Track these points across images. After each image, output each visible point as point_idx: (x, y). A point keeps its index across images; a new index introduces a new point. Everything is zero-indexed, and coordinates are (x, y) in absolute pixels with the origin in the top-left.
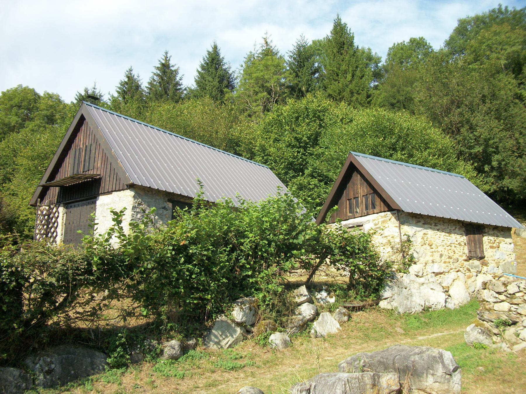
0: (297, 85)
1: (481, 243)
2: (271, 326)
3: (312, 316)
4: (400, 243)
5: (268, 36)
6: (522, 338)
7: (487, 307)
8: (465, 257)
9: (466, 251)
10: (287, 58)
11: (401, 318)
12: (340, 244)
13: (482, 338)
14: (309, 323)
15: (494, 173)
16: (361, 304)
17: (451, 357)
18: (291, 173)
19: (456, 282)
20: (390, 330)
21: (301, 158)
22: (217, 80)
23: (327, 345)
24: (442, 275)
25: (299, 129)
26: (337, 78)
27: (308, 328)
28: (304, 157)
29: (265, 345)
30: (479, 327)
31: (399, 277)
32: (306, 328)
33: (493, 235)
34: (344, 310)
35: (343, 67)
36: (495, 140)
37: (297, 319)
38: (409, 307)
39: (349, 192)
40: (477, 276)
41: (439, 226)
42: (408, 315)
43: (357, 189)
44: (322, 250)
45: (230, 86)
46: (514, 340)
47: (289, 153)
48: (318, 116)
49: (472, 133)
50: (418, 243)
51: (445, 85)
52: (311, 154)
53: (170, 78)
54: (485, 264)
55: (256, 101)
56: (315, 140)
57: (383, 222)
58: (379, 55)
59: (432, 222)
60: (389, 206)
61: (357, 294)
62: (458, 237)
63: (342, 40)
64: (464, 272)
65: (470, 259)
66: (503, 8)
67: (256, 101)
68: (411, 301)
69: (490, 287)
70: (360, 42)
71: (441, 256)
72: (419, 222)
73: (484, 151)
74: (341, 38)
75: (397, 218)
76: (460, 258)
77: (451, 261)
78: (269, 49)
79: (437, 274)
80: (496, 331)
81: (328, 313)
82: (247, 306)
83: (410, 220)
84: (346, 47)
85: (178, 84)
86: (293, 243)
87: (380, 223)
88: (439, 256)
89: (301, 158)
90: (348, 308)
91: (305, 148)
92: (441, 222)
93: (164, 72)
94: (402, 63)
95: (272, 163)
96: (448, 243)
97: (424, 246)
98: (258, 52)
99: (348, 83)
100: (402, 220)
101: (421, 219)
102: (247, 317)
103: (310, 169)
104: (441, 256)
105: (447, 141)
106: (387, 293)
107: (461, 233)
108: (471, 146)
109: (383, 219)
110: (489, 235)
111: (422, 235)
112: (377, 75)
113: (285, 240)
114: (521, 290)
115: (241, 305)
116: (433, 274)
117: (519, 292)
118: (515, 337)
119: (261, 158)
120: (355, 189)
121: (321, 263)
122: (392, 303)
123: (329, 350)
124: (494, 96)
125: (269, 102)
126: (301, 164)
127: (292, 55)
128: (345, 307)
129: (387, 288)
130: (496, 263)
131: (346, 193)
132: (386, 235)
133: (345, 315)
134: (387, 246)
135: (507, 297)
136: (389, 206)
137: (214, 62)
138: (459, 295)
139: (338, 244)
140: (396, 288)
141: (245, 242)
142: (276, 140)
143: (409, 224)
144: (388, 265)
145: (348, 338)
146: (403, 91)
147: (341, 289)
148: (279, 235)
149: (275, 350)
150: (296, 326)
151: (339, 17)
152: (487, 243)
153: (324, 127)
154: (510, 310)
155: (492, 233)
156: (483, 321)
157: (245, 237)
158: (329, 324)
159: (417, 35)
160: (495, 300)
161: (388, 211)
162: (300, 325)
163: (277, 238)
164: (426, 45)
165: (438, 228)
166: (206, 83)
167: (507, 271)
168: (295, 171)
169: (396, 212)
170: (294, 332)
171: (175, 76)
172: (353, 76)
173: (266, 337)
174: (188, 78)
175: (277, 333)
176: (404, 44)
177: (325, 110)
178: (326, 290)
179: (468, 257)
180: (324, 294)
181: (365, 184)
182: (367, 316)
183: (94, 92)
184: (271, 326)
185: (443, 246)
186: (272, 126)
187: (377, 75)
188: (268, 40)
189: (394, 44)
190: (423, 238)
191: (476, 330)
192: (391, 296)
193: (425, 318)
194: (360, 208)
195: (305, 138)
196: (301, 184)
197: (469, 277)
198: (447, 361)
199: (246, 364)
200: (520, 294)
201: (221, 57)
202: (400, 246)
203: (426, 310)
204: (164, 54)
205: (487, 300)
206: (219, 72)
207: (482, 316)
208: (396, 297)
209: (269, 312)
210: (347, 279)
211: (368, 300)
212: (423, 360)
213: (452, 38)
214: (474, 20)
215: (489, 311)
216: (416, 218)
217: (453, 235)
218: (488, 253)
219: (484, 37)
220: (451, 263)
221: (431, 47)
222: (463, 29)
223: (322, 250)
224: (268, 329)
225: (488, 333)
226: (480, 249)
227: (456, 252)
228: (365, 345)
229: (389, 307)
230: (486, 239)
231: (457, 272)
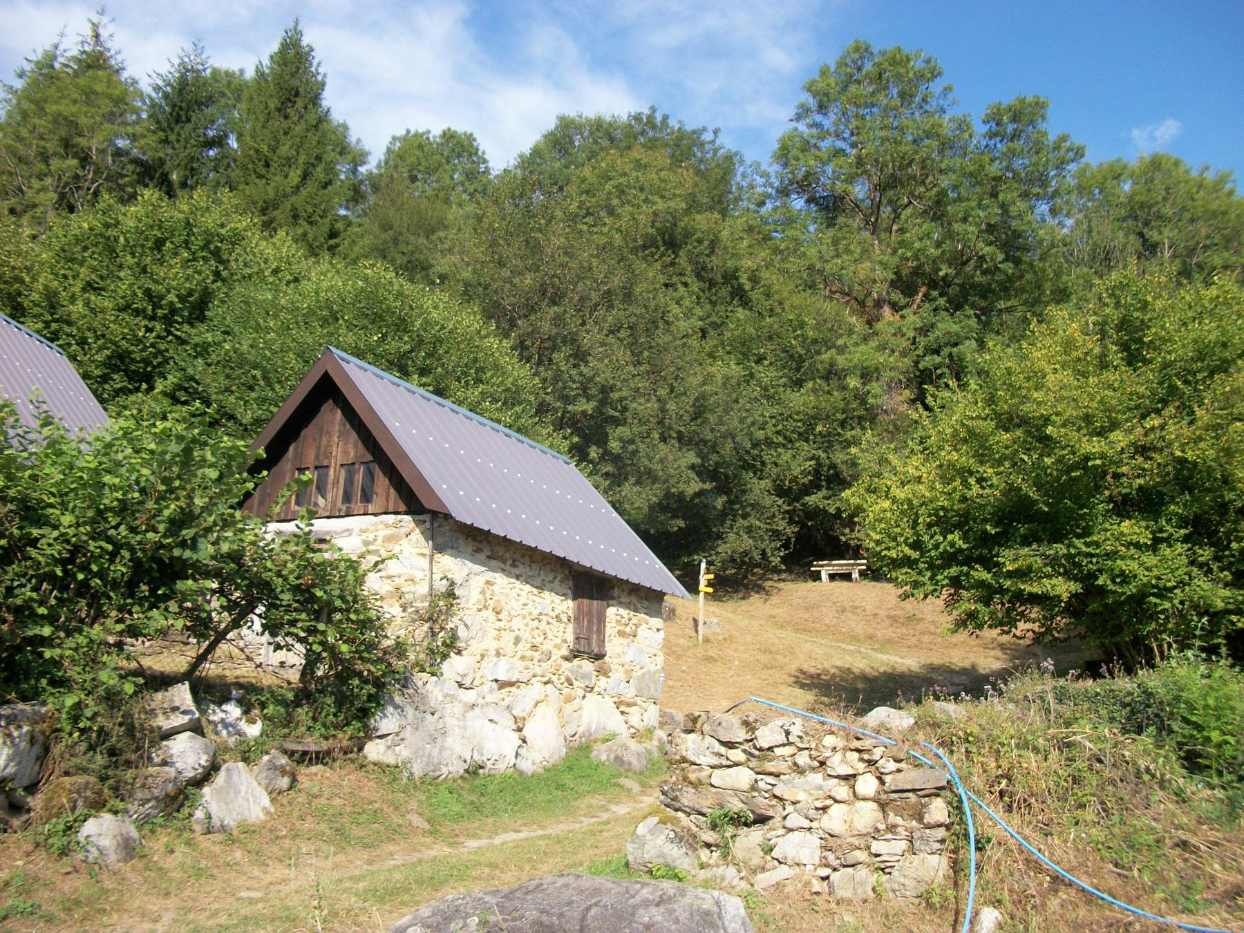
1: (601, 620)
2: (89, 793)
3: (200, 770)
4: (429, 598)
6: (780, 857)
7: (693, 777)
8: (565, 651)
9: (570, 637)
11: (415, 787)
12: (297, 578)
13: (677, 855)
14: (191, 790)
15: (609, 468)
16: (325, 745)
17: (742, 912)
18: (118, 381)
19: (541, 707)
20: (397, 820)
21: (153, 345)
23: (238, 854)
24: (513, 689)
26: (264, 171)
27: (187, 803)
29: (64, 852)
30: (669, 825)
31: (420, 684)
32: (182, 805)
33: (627, 606)
34: (284, 760)
35: (285, 150)
36: (624, 393)
37: (159, 778)
38: (436, 761)
39: (306, 448)
40: (584, 697)
41: (521, 567)
42: (431, 781)
43: (329, 445)
44: (251, 588)
46: (756, 861)
48: (215, 250)
49: (575, 366)
50: (471, 602)
51: (535, 248)
52: (183, 342)
54: (603, 672)
55: (41, 177)
56: (198, 309)
57: (388, 539)
58: (367, 145)
59: (507, 555)
60: (412, 500)
61: (314, 719)
62: (557, 599)
63: (294, 82)
64: (560, 686)
65: (575, 657)
66: (659, 117)
67: (41, 177)
68: (443, 748)
69: (706, 728)
70: (338, 103)
71: (517, 640)
72: (479, 550)
73: (599, 410)
74: (292, 83)
75: (429, 533)
76: (555, 651)
77: (537, 655)
78: (101, 53)
79: (503, 685)
80: (709, 836)
81: (241, 764)
82: (25, 729)
83: (461, 542)
84: (300, 103)
86: (179, 558)
87: (379, 541)
88: (512, 640)
89: (153, 345)
90: (291, 754)
91: (168, 321)
92: (527, 560)
94: (413, 179)
95: (69, 345)
96: (536, 612)
97: (484, 613)
98: (68, 54)
99: (289, 190)
100: (440, 540)
101: (485, 543)
102: (19, 763)
103: (172, 379)
104: (517, 640)
105: (520, 373)
106: (387, 722)
107: (565, 591)
108: (568, 397)
109: (388, 532)
110: (620, 604)
111: (482, 585)
112: (356, 195)
113: (162, 546)
114: (791, 739)
115: (8, 724)
116: (495, 685)
117: (784, 745)
118: (762, 854)
119: (40, 325)
120: (324, 443)
121: (235, 624)
122: (397, 748)
123: (246, 869)
124: (628, 296)
125: (78, 188)
126: (147, 362)
127: (161, 83)
128: (285, 752)
129: (390, 709)
130: (626, 672)
131: (296, 450)
132: (390, 572)
133: (284, 772)
134: (391, 601)
135: (751, 755)
136: (412, 500)
138: (546, 744)
139: (291, 578)
140: (410, 711)
141: (43, 536)
143: (457, 552)
144: (400, 649)
145: (293, 838)
146: (408, 244)
147: (283, 702)
148: (147, 531)
149: (95, 869)
150: (156, 798)
151: (299, 28)
152: (613, 624)
153: (224, 280)
154: (754, 788)
155: (627, 600)
156: (676, 810)
158: (241, 796)
159: (460, 128)
160: (715, 761)
161: (406, 513)
162: (167, 795)
163: (139, 538)
164: (476, 154)
165: (517, 571)
167: (646, 693)
168: (132, 376)
169: (426, 517)
170: (148, 815)
172: (305, 177)
173: (70, 828)
175: (107, 817)
176: (428, 138)
177: (236, 239)
178: (240, 702)
179: (572, 651)
180: (233, 711)
181: (354, 435)
182: (336, 778)
184: (89, 793)
185: (524, 617)
186: (85, 249)
187: (356, 195)
188: (102, 31)
189: (408, 131)
190: (483, 592)
191: (662, 832)
192: (397, 730)
193: (471, 791)
194: (329, 496)
195: (172, 297)
197: (569, 699)
198: (733, 925)
199: (12, 907)
200: (788, 751)
202: (427, 604)
203: (473, 771)
205: (692, 758)
207: (675, 799)
208: (407, 733)
209: (85, 753)
210: (294, 676)
211: (340, 735)
212: (677, 921)
213: (536, 152)
214: (591, 126)
215: (695, 787)
216: (474, 539)
217: (546, 594)
218: (614, 646)
219: (613, 166)
220: (535, 661)
221: (485, 161)
222: (562, 139)
223: (251, 588)
224: (80, 803)
225: (689, 840)
226: (598, 636)
227: (550, 635)
228: (341, 858)
229: (391, 760)
230: (614, 614)
231: (546, 683)
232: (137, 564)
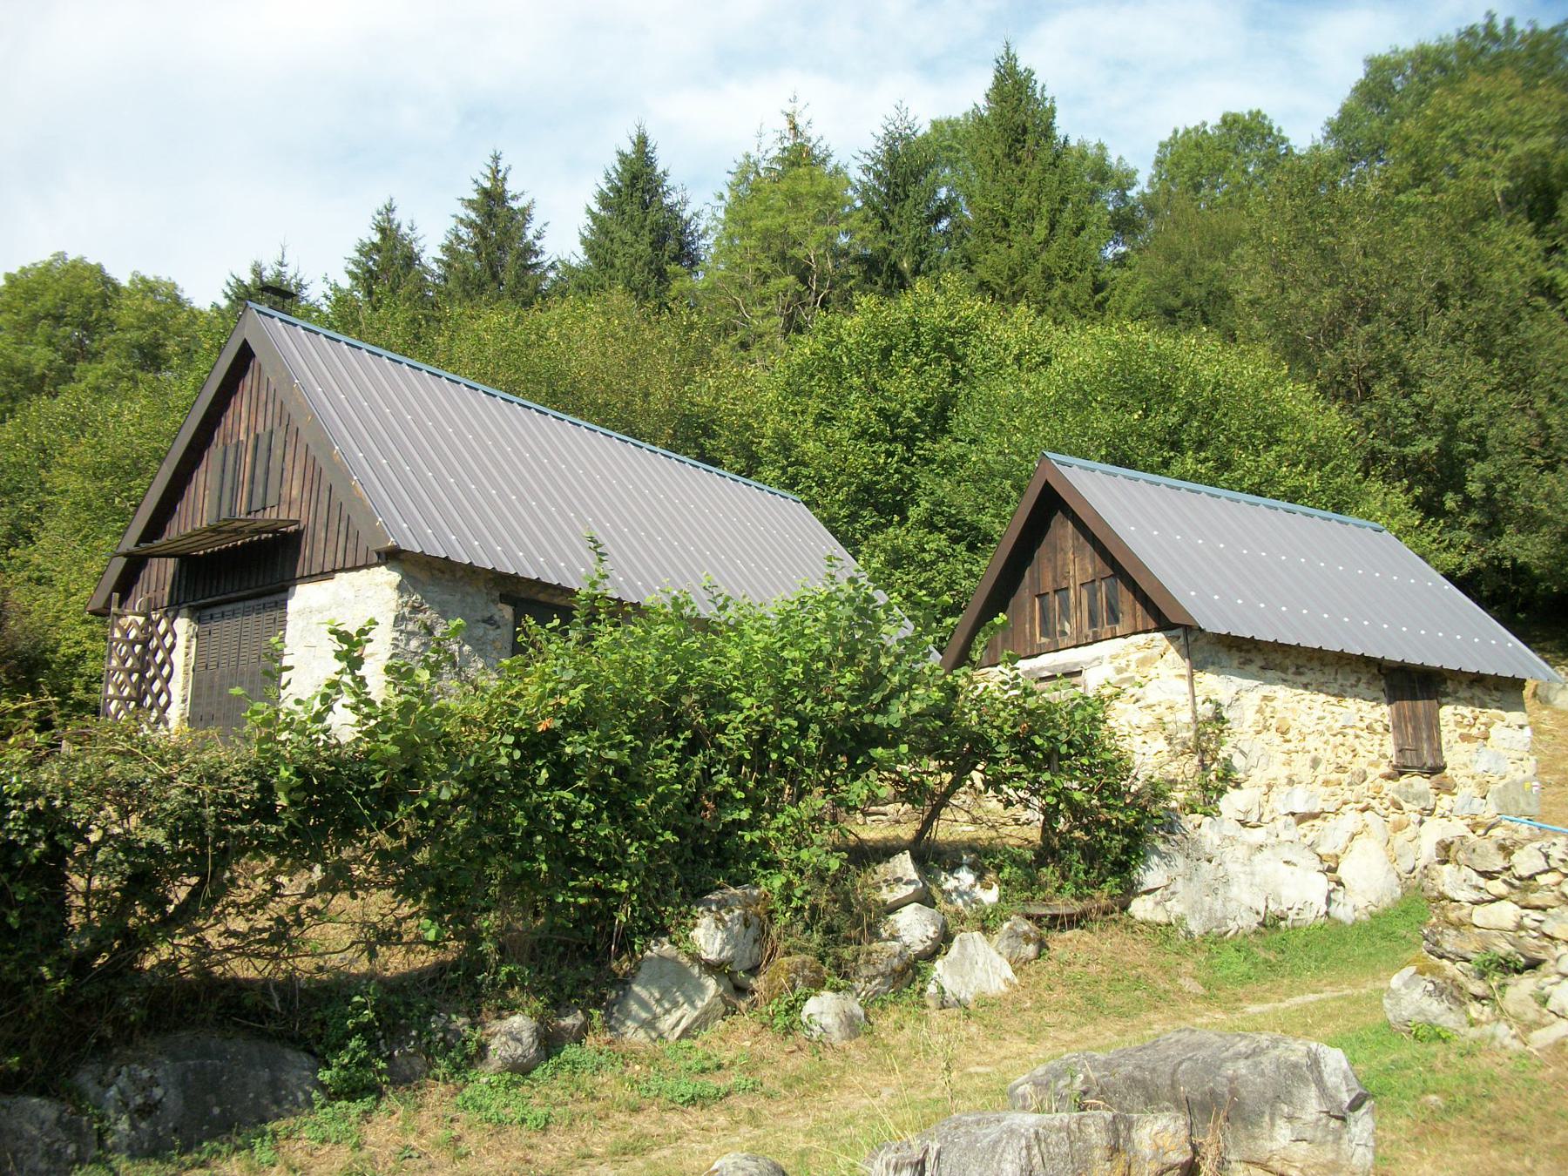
0: (887, 253)
1: (1434, 725)
2: (807, 972)
3: (929, 943)
4: (1193, 727)
5: (799, 106)
6: (1556, 1009)
7: (1452, 916)
8: (1385, 769)
9: (1390, 749)
10: (855, 174)
11: (1195, 949)
12: (1013, 727)
13: (1436, 1008)
14: (921, 964)
15: (1474, 517)
16: (1077, 907)
17: (1345, 1065)
18: (868, 517)
19: (1358, 841)
20: (1163, 985)
21: (897, 471)
22: (647, 240)
23: (974, 1029)
24: (1317, 822)
25: (890, 386)
26: (1004, 233)
27: (919, 978)
28: (907, 470)
29: (789, 1030)
30: (1428, 976)
31: (1189, 827)
32: (913, 980)
33: (1469, 702)
34: (1026, 926)
35: (1024, 201)
36: (1477, 419)
37: (885, 952)
38: (1219, 915)
39: (1041, 573)
40: (1421, 822)
41: (1309, 673)
42: (1215, 940)
43: (1065, 565)
44: (959, 746)
45: (687, 256)
46: (1531, 1015)
47: (861, 458)
48: (947, 346)
49: (1406, 396)
50: (1246, 725)
51: (1327, 255)
52: (928, 461)
53: (506, 232)
54: (1446, 788)
55: (763, 301)
56: (938, 417)
57: (1143, 662)
58: (1131, 163)
59: (1288, 662)
60: (1160, 615)
61: (1064, 877)
62: (1366, 706)
63: (1018, 119)
64: (1384, 812)
65: (1402, 774)
66: (1500, 24)
67: (763, 301)
68: (1226, 900)
69: (1461, 856)
70: (1073, 126)
71: (1315, 763)
72: (1250, 661)
73: (1444, 451)
74: (1017, 115)
75: (1184, 650)
76: (1370, 770)
77: (1345, 778)
78: (802, 145)
79: (1302, 818)
80: (1477, 987)
81: (977, 934)
82: (737, 912)
83: (1223, 656)
84: (1030, 140)
85: (530, 250)
86: (872, 724)
87: (1133, 666)
88: (1309, 763)
89: (897, 471)
90: (1037, 920)
91: (909, 442)
92: (1316, 664)
93: (490, 216)
94: (1197, 187)
95: (810, 488)
96: (1337, 726)
97: (1265, 735)
98: (769, 156)
99: (1037, 248)
100: (1198, 657)
101: (1254, 652)
102: (735, 946)
103: (924, 504)
104: (1315, 763)
105: (1332, 421)
106: (1152, 875)
107: (1375, 695)
108: (1403, 436)
109: (1141, 655)
110: (1458, 700)
111: (1257, 701)
112: (1124, 224)
113: (850, 715)
114: (1553, 864)
115: (719, 909)
116: (1291, 819)
117: (1546, 872)
118: (1536, 1006)
119: (778, 472)
120: (1059, 563)
121: (956, 784)
122: (1168, 904)
123: (979, 1044)
124: (1472, 287)
125: (803, 305)
126: (896, 490)
127: (870, 163)
128: (1029, 917)
129: (1155, 859)
130: (1480, 785)
131: (1032, 577)
132: (1150, 702)
133: (1028, 940)
134: (1154, 734)
135: (1511, 885)
136: (1160, 615)
137: (637, 184)
138: (1370, 881)
139: (1006, 728)
140: (1180, 860)
141: (730, 721)
142: (823, 419)
143: (1220, 669)
144: (1157, 792)
145: (1038, 1010)
146: (1203, 271)
147: (1016, 861)
148: (833, 701)
149: (820, 1045)
150: (883, 974)
151: (1012, 52)
152: (1452, 726)
153: (964, 379)
154: (1520, 926)
155: (1467, 694)
156: (1441, 957)
157: (730, 707)
158: (980, 967)
159: (1242, 105)
160: (1475, 896)
161: (1157, 630)
162: (893, 970)
163: (826, 709)
164: (1270, 134)
165: (1304, 680)
166: (615, 247)
167: (1513, 810)
168: (880, 509)
169: (1179, 632)
170: (876, 992)
171: (522, 227)
172: (1052, 227)
173: (793, 1007)
174: (561, 233)
175: (827, 995)
176: (1205, 132)
177: (969, 329)
178: (972, 867)
179: (1395, 767)
180: (966, 877)
181: (1089, 548)
182: (1095, 943)
183: (279, 274)
184: (807, 972)
185: (1322, 734)
186: (812, 376)
187: (1124, 224)
188: (798, 121)
189: (1176, 132)
190: (1260, 711)
191: (1418, 985)
192: (1166, 882)
193: (1267, 948)
194: (1073, 621)
195: (908, 413)
196: (896, 550)
197: (1399, 828)
198: (1333, 1079)
199: (734, 1085)
200: (1551, 878)
201: (659, 170)
202: (1191, 733)
203: (1270, 924)
204: (489, 161)
205: (1451, 894)
206: (654, 216)
207: (1437, 943)
208: (1179, 885)
209: (803, 932)
210: (1035, 834)
211: (1097, 894)
212: (1262, 1074)
213: (1347, 115)
214: (1413, 60)
215: (1457, 928)
216: (1240, 650)
217: (1349, 701)
218: (1455, 755)
219: (1442, 111)
220: (1344, 785)
221: (1284, 140)
222: (1380, 87)
223: (959, 746)
224: (799, 982)
225: (1454, 994)
226: (1431, 745)
227: (1361, 751)
228: (1089, 1030)
229: (1161, 917)
230: (1449, 714)
231: (1363, 810)
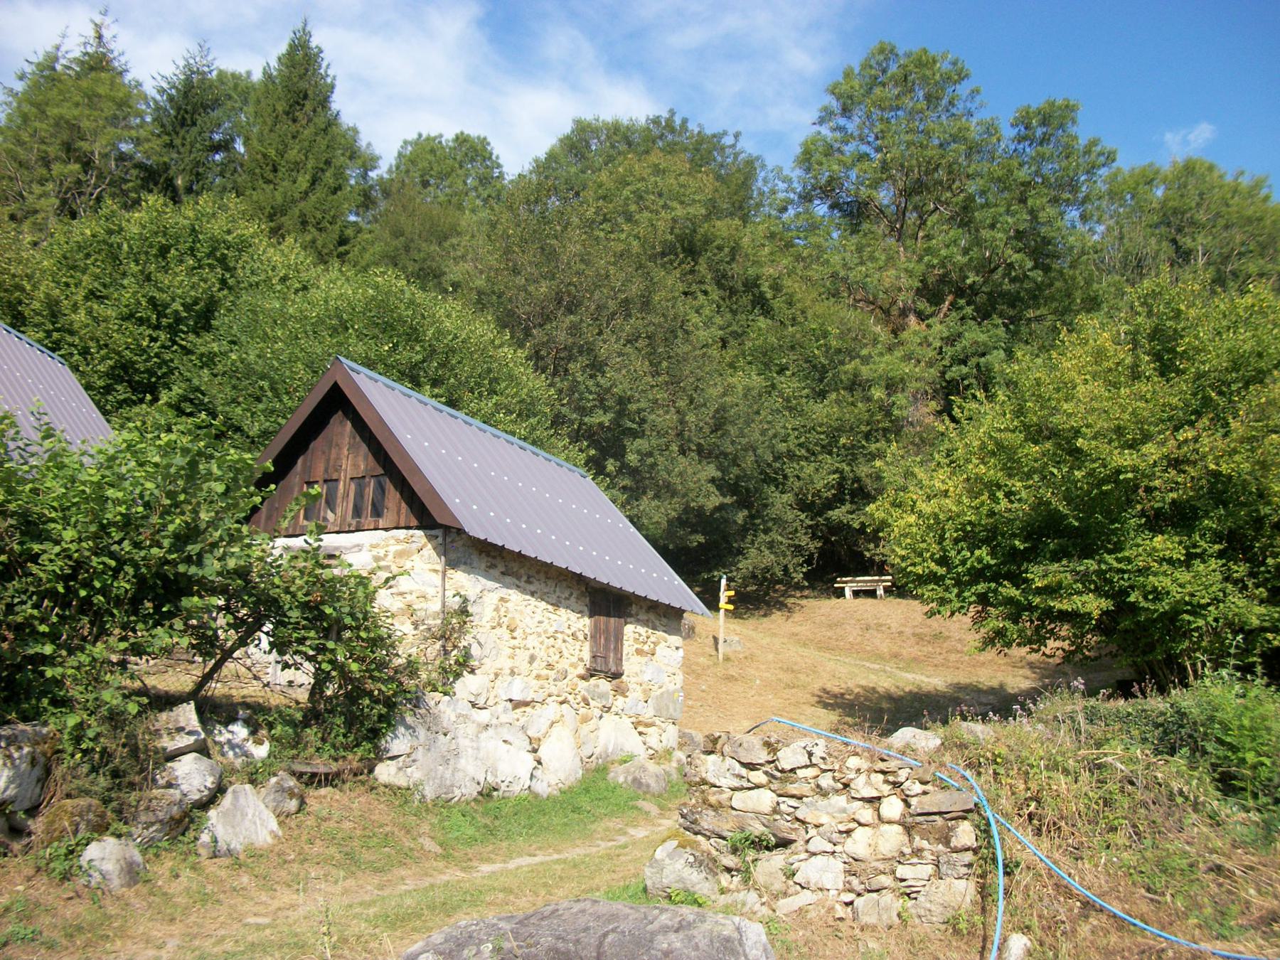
1: (619, 638)
2: (91, 816)
3: (206, 793)
4: (441, 616)
6: (802, 881)
7: (713, 799)
8: (581, 670)
9: (587, 656)
11: (427, 810)
12: (306, 595)
13: (696, 879)
14: (196, 813)
15: (627, 482)
16: (334, 767)
17: (764, 938)
18: (122, 392)
19: (557, 727)
20: (408, 843)
21: (157, 355)
23: (245, 879)
24: (528, 709)
26: (271, 176)
27: (193, 827)
29: (66, 877)
30: (688, 849)
31: (432, 703)
32: (187, 828)
33: (645, 623)
34: (292, 782)
35: (293, 154)
36: (643, 405)
37: (164, 801)
38: (448, 783)
39: (314, 461)
40: (601, 717)
41: (537, 583)
42: (443, 804)
43: (338, 458)
44: (258, 605)
46: (778, 886)
48: (221, 257)
49: (591, 377)
50: (485, 620)
51: (550, 255)
52: (188, 352)
54: (621, 691)
55: (42, 182)
56: (204, 318)
57: (400, 554)
58: (378, 149)
59: (522, 571)
60: (424, 514)
61: (323, 740)
62: (573, 616)
63: (303, 85)
64: (576, 706)
65: (592, 676)
66: (678, 121)
67: (42, 182)
68: (455, 770)
69: (727, 749)
70: (348, 106)
71: (532, 659)
72: (493, 566)
73: (616, 422)
74: (301, 86)
75: (442, 548)
76: (571, 670)
77: (552, 674)
78: (104, 55)
79: (517, 704)
80: (730, 861)
81: (248, 787)
82: (26, 750)
83: (475, 557)
84: (308, 106)
86: (185, 574)
87: (390, 557)
88: (527, 659)
89: (157, 355)
90: (299, 776)
91: (173, 330)
92: (542, 576)
94: (425, 184)
95: (72, 355)
96: (551, 630)
97: (498, 631)
98: (70, 56)
99: (297, 196)
100: (453, 556)
101: (499, 559)
102: (20, 785)
103: (177, 390)
104: (532, 659)
105: (535, 384)
106: (398, 743)
107: (581, 608)
108: (584, 408)
109: (400, 547)
110: (638, 621)
111: (496, 602)
112: (367, 201)
113: (167, 562)
114: (814, 761)
115: (8, 745)
116: (509, 705)
117: (806, 767)
118: (784, 879)
119: (41, 335)
120: (333, 456)
121: (242, 642)
122: (409, 770)
123: (253, 894)
124: (646, 305)
125: (80, 194)
126: (151, 372)
127: (165, 86)
128: (293, 773)
129: (402, 729)
130: (644, 691)
131: (304, 463)
132: (402, 589)
133: (292, 795)
134: (402, 619)
135: (773, 776)
136: (424, 514)
138: (562, 765)
139: (300, 594)
140: (422, 732)
141: (44, 552)
143: (470, 568)
144: (412, 668)
145: (302, 862)
146: (419, 251)
147: (291, 722)
148: (151, 546)
149: (98, 894)
150: (161, 821)
151: (308, 29)
152: (631, 642)
153: (230, 288)
154: (775, 811)
155: (645, 617)
156: (696, 834)
158: (248, 819)
159: (473, 131)
160: (736, 783)
161: (418, 528)
162: (172, 818)
163: (143, 553)
164: (490, 158)
165: (532, 588)
167: (664, 713)
168: (136, 387)
169: (438, 532)
170: (152, 838)
172: (314, 182)
173: (72, 852)
175: (110, 841)
176: (440, 142)
177: (243, 246)
178: (247, 722)
179: (588, 670)
180: (240, 731)
181: (364, 448)
182: (346, 801)
184: (91, 816)
185: (539, 635)
186: (88, 256)
187: (367, 201)
188: (105, 32)
189: (420, 135)
190: (497, 609)
191: (681, 857)
192: (408, 751)
193: (485, 814)
194: (339, 511)
195: (177, 306)
197: (585, 720)
198: (754, 952)
199: (13, 934)
200: (810, 772)
202: (439, 622)
203: (487, 793)
205: (712, 780)
207: (694, 822)
208: (419, 754)
209: (87, 775)
210: (303, 695)
211: (350, 757)
212: (697, 948)
213: (552, 156)
214: (608, 129)
215: (716, 810)
216: (488, 555)
217: (562, 611)
218: (631, 665)
219: (630, 171)
220: (551, 680)
221: (499, 166)
222: (579, 143)
223: (258, 605)
224: (82, 826)
225: (709, 865)
226: (616, 654)
227: (565, 653)
228: (351, 882)
229: (402, 782)
230: (632, 632)
231: (562, 703)
232: (141, 581)
